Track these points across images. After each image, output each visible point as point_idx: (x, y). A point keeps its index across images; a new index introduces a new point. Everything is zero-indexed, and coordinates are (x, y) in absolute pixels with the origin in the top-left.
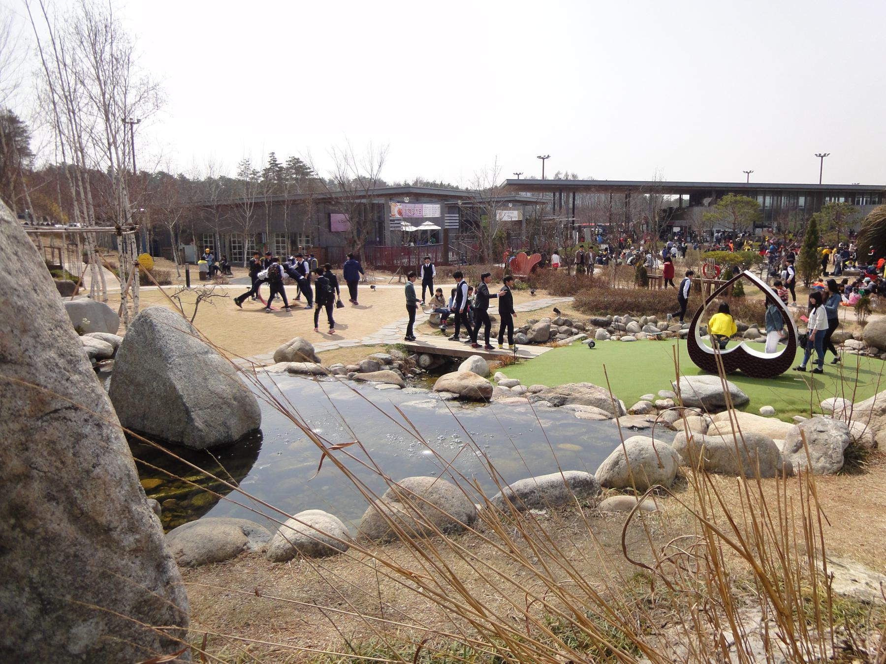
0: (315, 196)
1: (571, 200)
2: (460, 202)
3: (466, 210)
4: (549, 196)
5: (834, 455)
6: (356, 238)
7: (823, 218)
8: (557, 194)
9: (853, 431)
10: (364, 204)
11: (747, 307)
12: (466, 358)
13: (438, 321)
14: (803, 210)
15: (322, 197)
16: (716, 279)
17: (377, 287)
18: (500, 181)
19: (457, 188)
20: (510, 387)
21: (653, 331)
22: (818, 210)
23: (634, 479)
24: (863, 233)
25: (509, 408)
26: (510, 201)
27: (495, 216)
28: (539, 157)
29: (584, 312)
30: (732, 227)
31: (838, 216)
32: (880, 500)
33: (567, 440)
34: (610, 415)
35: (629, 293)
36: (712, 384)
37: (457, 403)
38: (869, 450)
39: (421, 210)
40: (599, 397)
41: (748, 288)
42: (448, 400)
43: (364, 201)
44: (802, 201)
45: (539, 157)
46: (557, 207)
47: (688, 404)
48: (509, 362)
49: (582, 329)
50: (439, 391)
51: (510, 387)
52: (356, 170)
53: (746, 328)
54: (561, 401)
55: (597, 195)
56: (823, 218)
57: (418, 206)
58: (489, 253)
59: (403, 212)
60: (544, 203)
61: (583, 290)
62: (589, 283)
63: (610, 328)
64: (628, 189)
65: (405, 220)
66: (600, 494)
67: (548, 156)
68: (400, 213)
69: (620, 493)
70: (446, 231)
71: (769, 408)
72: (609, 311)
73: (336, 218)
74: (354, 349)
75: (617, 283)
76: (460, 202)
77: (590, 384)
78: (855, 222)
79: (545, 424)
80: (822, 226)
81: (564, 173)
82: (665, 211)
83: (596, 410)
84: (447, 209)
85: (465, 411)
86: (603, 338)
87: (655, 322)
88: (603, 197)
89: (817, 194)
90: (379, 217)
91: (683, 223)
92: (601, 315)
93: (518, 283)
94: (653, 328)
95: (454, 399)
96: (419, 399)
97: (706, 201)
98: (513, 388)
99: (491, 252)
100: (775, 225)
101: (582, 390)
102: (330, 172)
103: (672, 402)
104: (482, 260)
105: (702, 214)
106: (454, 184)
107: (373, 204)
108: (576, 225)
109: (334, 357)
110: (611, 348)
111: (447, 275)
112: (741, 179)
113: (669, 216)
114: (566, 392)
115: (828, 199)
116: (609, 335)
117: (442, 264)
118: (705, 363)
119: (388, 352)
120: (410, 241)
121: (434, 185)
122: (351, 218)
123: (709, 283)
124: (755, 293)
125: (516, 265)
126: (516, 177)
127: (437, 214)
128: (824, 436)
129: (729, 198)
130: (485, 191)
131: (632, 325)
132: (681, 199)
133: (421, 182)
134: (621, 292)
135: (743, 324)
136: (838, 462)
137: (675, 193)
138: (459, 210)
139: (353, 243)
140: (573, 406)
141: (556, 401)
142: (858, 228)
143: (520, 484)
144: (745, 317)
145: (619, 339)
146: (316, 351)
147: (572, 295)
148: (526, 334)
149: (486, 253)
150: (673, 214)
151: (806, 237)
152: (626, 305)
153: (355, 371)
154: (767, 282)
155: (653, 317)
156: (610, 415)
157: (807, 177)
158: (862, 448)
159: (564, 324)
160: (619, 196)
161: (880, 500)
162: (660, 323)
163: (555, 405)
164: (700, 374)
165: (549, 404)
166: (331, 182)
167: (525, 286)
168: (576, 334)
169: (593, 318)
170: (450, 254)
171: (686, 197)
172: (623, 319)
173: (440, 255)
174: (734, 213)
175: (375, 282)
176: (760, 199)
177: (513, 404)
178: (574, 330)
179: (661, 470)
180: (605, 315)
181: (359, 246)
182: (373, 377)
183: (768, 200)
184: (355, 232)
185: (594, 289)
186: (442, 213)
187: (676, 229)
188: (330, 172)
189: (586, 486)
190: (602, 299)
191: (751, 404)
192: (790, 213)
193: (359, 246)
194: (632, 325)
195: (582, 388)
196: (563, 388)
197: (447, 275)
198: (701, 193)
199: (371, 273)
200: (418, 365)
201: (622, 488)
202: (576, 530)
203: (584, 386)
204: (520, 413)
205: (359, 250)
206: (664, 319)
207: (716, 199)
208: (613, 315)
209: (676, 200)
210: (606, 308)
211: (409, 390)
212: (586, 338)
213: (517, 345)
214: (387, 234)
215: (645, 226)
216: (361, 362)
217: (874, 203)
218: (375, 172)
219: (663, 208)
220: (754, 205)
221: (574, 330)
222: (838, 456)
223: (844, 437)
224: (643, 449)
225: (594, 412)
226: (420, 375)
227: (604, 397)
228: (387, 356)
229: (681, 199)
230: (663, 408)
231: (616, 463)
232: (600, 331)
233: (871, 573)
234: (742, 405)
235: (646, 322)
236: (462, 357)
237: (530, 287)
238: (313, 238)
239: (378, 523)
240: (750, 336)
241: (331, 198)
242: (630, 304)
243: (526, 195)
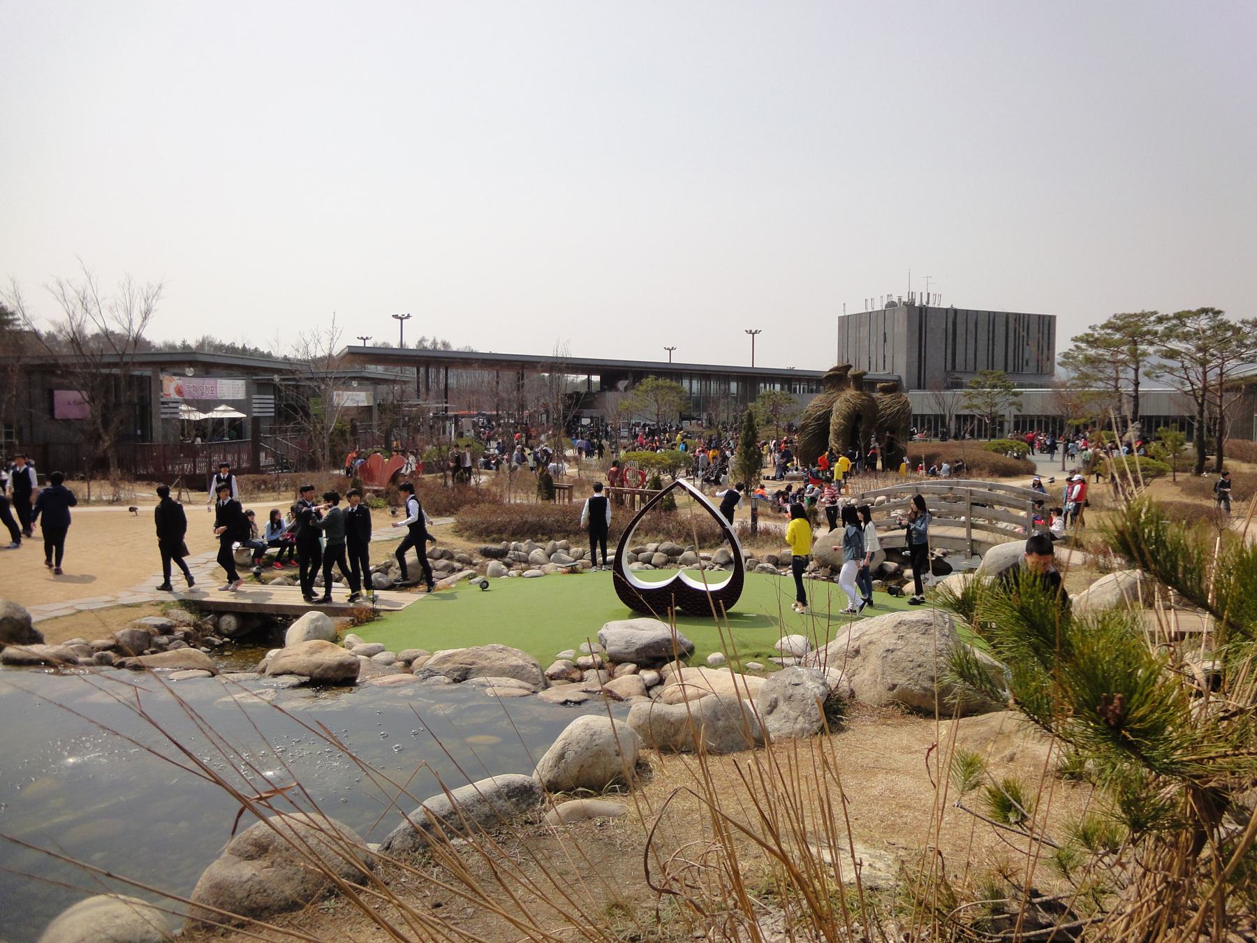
0: (24, 361)
1: (442, 376)
2: (276, 378)
3: (287, 391)
4: (411, 372)
5: (813, 713)
6: (101, 430)
7: (759, 408)
8: (422, 370)
9: (829, 680)
10: (116, 377)
11: (680, 523)
12: (297, 617)
13: (249, 560)
14: (736, 398)
15: (37, 362)
16: (640, 488)
17: (140, 508)
18: (339, 348)
19: (269, 355)
20: (370, 656)
21: (563, 562)
22: (753, 400)
23: (592, 776)
24: (804, 427)
25: (390, 691)
26: (354, 378)
27: (331, 399)
28: (396, 316)
29: (469, 539)
30: (655, 418)
31: (776, 406)
32: (867, 761)
33: (480, 729)
34: (533, 688)
35: (531, 509)
36: (652, 629)
37: (308, 692)
38: (847, 701)
39: (214, 389)
40: (514, 663)
41: (680, 499)
42: (294, 687)
43: (115, 371)
44: (734, 386)
45: (396, 316)
46: (424, 388)
47: (616, 660)
48: (363, 618)
49: (469, 563)
50: (275, 675)
51: (370, 656)
52: (104, 318)
53: (680, 552)
54: (463, 676)
55: (478, 373)
56: (759, 408)
57: (209, 382)
58: (323, 455)
59: (185, 390)
60: (405, 382)
61: (467, 507)
62: (475, 496)
63: (507, 560)
64: (521, 366)
65: (188, 402)
66: (543, 802)
67: (409, 316)
68: (179, 391)
69: (571, 797)
70: (256, 421)
71: (719, 655)
72: (504, 536)
73: (62, 396)
74: (104, 613)
75: (512, 495)
76: (276, 378)
77: (501, 646)
78: (794, 415)
79: (443, 710)
80: (759, 419)
81: (431, 340)
82: (570, 396)
83: (514, 682)
84: (254, 388)
85: (322, 702)
86: (498, 574)
87: (567, 549)
88: (486, 376)
89: (751, 379)
90: (142, 398)
91: (595, 413)
92: (494, 541)
93: (370, 498)
94: (565, 556)
95: (302, 685)
96: (248, 690)
97: (622, 384)
98: (375, 657)
99: (327, 453)
100: (705, 416)
101: (490, 655)
102: (53, 323)
103: (598, 659)
104: (313, 465)
105: (618, 401)
106: (264, 349)
107: (132, 376)
108: (450, 413)
109: (67, 629)
110: (510, 587)
111: (259, 488)
112: (661, 357)
113: (576, 404)
114: (470, 661)
115: (762, 385)
116: (506, 570)
117: (249, 471)
118: (641, 603)
119: (165, 614)
120: (197, 436)
121: (232, 350)
122: (92, 399)
123: (633, 494)
124: (689, 505)
125: (368, 474)
126: (360, 343)
127: (241, 395)
128: (800, 690)
129: (649, 381)
130: (316, 361)
131: (537, 553)
132: (589, 380)
133: (211, 344)
134: (519, 509)
135: (677, 547)
136: (818, 721)
137: (583, 373)
138: (275, 389)
139: (96, 438)
140: (481, 679)
141: (456, 675)
142: (798, 423)
143: (437, 802)
144: (679, 537)
145: (520, 575)
146: (33, 620)
147: (451, 514)
148: (387, 574)
149: (319, 454)
150: (580, 400)
151: (743, 432)
152: (527, 526)
153: (106, 649)
154: (702, 490)
155: (563, 542)
156: (533, 688)
157: (740, 360)
158: (839, 700)
159: (441, 557)
160: (509, 376)
161: (867, 761)
162: (573, 550)
163: (455, 681)
164: (632, 616)
165: (447, 680)
166: (51, 337)
167: (381, 502)
168: (460, 570)
169: (483, 546)
170: (263, 455)
171: (596, 378)
172: (524, 545)
173: (245, 457)
174: (656, 401)
175: (135, 501)
176: (686, 383)
177: (395, 685)
178: (457, 565)
179: (620, 759)
180: (499, 541)
181: (107, 442)
182: (163, 660)
183: (696, 385)
184: (99, 421)
185: (482, 505)
186: (248, 393)
187: (585, 421)
188: (53, 323)
189: (523, 794)
190: (493, 519)
191: (697, 652)
192: (722, 401)
193: (107, 442)
194: (537, 553)
195: (493, 652)
196: (460, 653)
197: (259, 488)
198: (616, 374)
199: (127, 486)
200: (218, 631)
201: (570, 791)
202: (519, 859)
203: (493, 649)
204: (407, 697)
205: (105, 451)
206: (577, 543)
207: (634, 383)
208: (509, 541)
209: (583, 382)
210: (500, 531)
211: (223, 678)
212: (474, 576)
213: (376, 592)
214: (157, 425)
215: (544, 416)
216: (118, 634)
217: (812, 391)
218: (135, 328)
219: (569, 392)
220: (679, 392)
221: (457, 565)
222: (817, 712)
223: (822, 688)
224: (595, 733)
225: (511, 686)
226: (222, 647)
227: (521, 662)
228: (163, 621)
229: (589, 380)
230: (588, 668)
231: (561, 756)
232: (493, 564)
233: (871, 851)
234: (686, 655)
235: (554, 551)
236: (290, 615)
237: (389, 504)
238: (20, 429)
239: (221, 899)
240: (687, 562)
241: (57, 366)
242: (532, 525)
243: (377, 370)
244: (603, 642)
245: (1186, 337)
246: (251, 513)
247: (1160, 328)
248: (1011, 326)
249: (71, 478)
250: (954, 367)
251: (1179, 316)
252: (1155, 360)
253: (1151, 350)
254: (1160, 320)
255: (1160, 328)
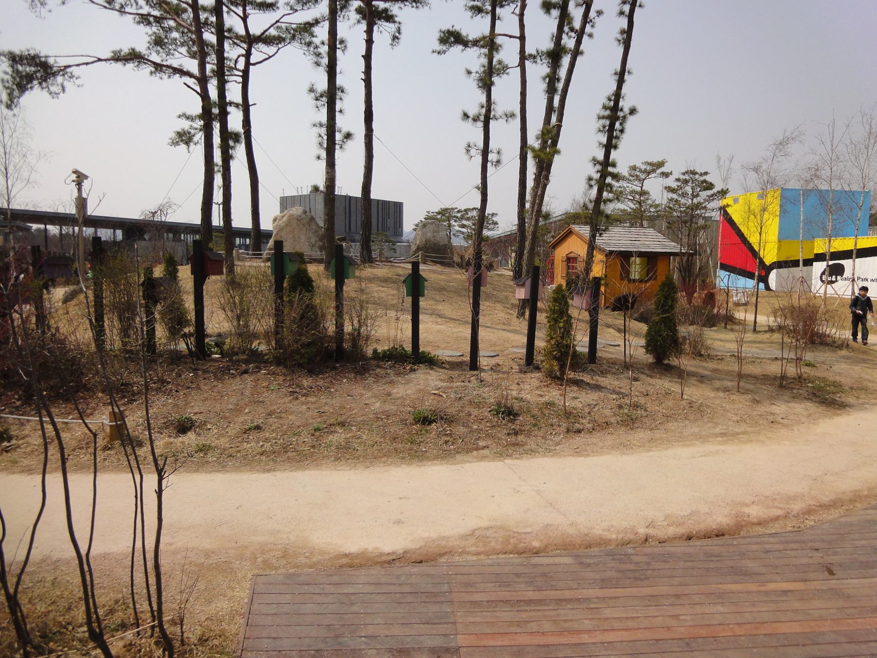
244: (80, 598)
245: (468, 219)
246: (286, 202)
247: (459, 215)
248: (380, 207)
249: (574, 223)
250: (350, 230)
251: (466, 210)
252: (457, 228)
253: (456, 224)
254: (459, 212)
255: (459, 215)
